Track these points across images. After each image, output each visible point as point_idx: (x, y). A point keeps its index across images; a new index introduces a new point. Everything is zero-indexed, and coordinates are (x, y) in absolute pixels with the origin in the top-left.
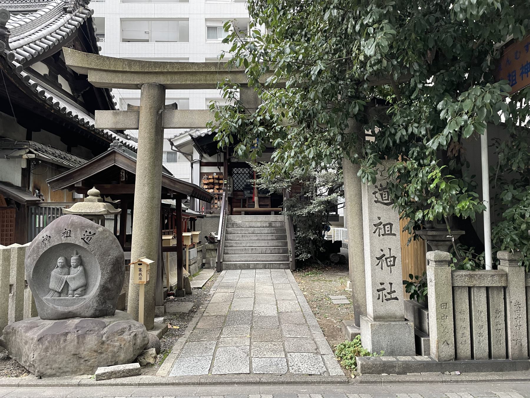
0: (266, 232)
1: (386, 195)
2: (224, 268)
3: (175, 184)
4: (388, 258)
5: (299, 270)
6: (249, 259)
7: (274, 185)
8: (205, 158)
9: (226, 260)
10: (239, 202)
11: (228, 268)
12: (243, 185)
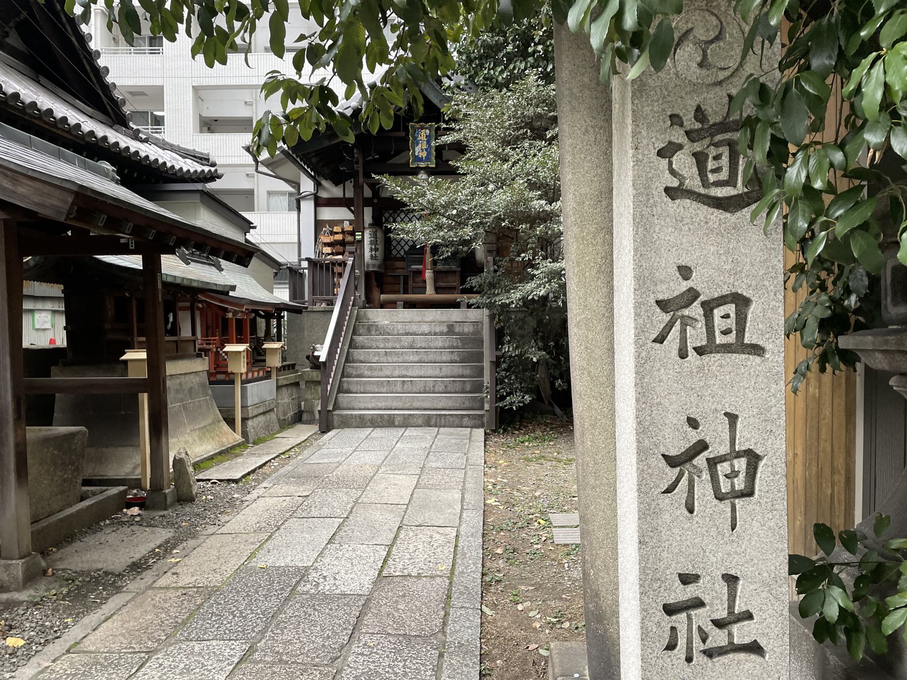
0: (440, 344)
1: (725, 161)
2: (335, 423)
3: (14, 181)
4: (722, 459)
5: (505, 430)
6: (395, 404)
7: (441, 233)
8: (325, 189)
9: (344, 405)
10: (392, 279)
11: (346, 423)
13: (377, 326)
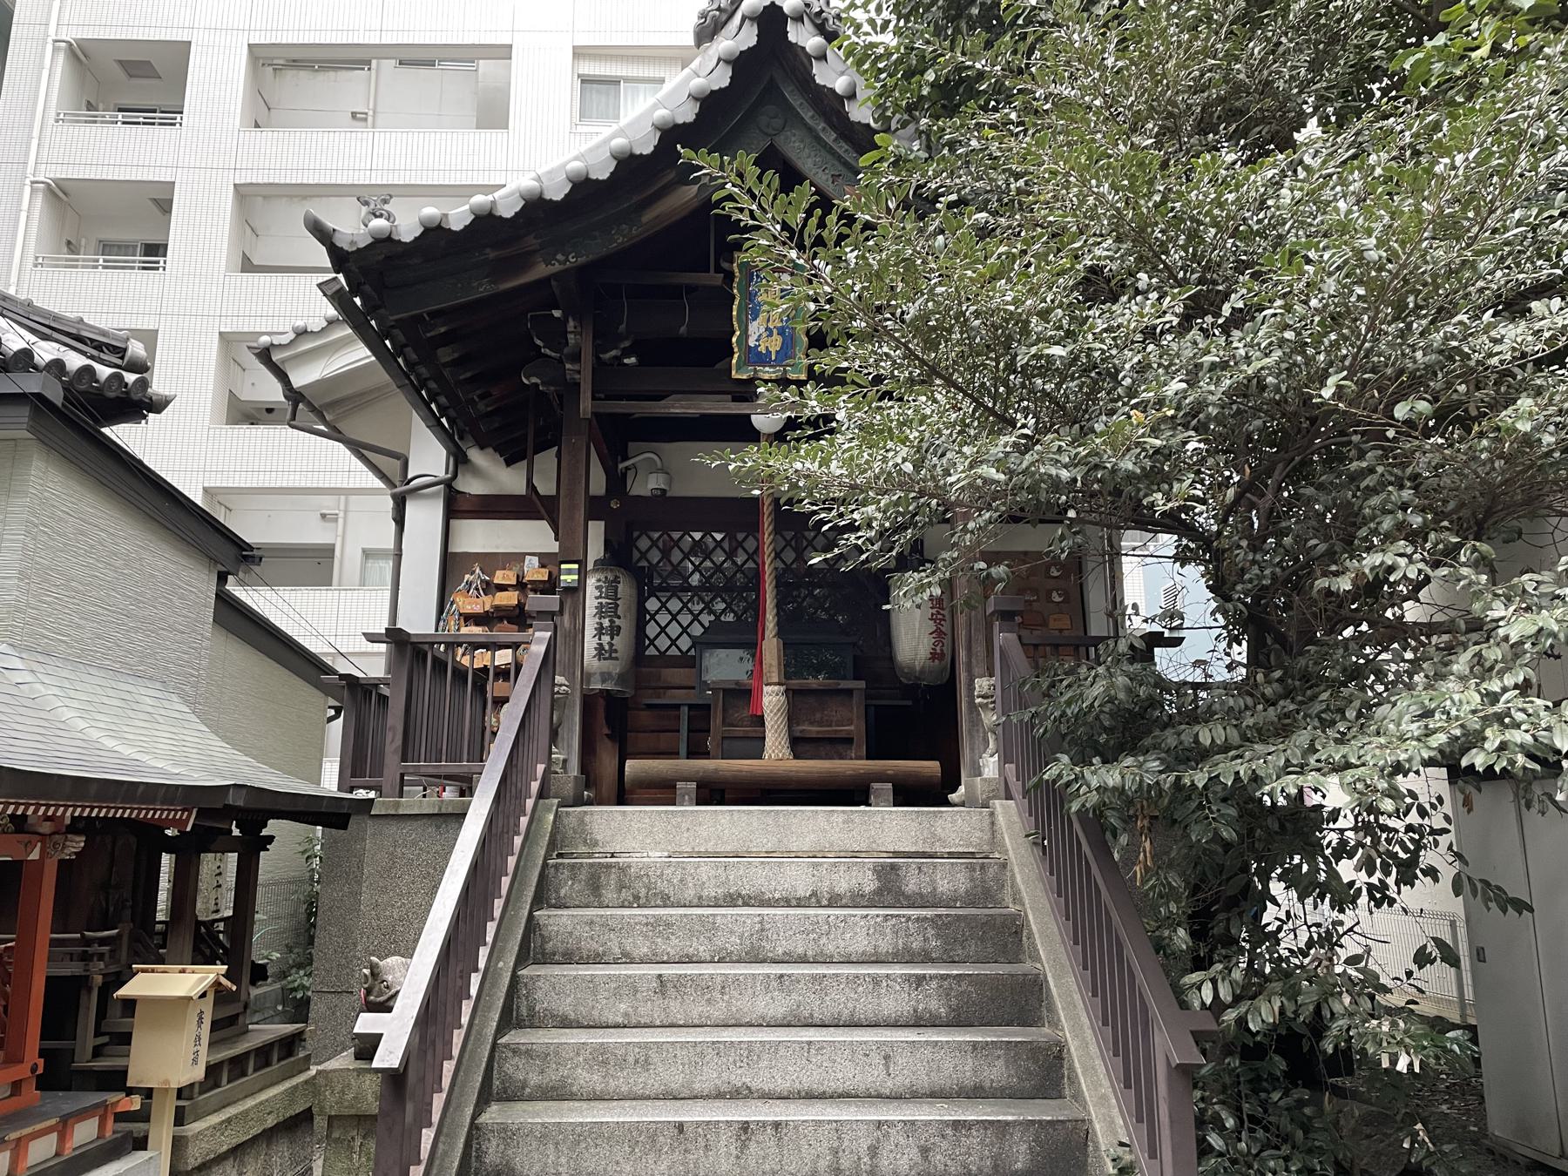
8: (476, 472)
12: (697, 630)
13: (623, 869)
